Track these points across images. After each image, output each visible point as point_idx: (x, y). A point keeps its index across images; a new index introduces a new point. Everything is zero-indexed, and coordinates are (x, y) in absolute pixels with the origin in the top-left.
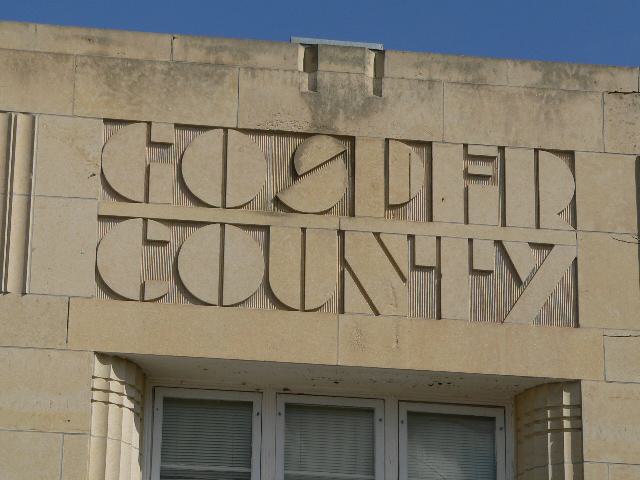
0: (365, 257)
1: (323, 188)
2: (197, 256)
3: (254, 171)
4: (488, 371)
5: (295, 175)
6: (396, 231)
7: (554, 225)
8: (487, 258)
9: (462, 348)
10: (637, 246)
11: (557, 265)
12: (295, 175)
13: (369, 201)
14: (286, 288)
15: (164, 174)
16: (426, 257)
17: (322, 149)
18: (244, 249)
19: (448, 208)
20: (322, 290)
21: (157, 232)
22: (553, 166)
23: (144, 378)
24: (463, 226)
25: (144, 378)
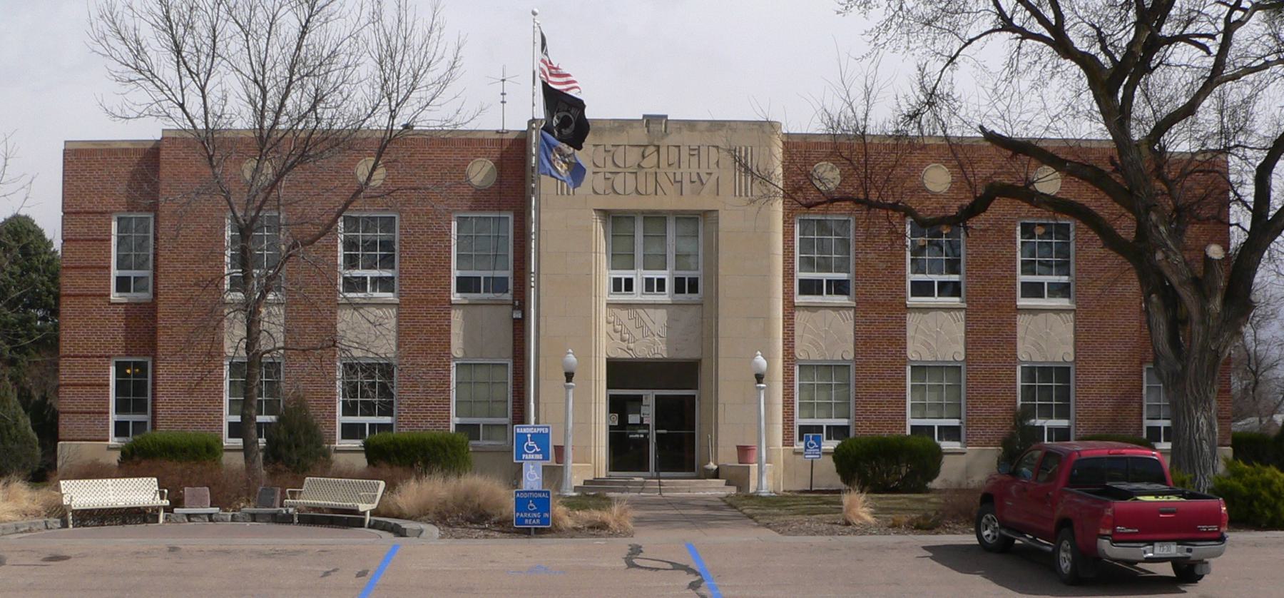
0: (663, 179)
1: (651, 161)
2: (619, 181)
3: (634, 156)
4: (994, 586)
5: (643, 157)
6: (670, 171)
7: (713, 166)
8: (695, 178)
9: (689, 203)
10: (363, 455)
11: (714, 178)
12: (643, 157)
13: (663, 163)
14: (642, 190)
15: (609, 162)
16: (678, 178)
17: (652, 149)
18: (630, 178)
19: (684, 165)
20: (651, 189)
21: (608, 175)
22: (713, 150)
23: (606, 214)
24: (688, 169)
25: (606, 214)
